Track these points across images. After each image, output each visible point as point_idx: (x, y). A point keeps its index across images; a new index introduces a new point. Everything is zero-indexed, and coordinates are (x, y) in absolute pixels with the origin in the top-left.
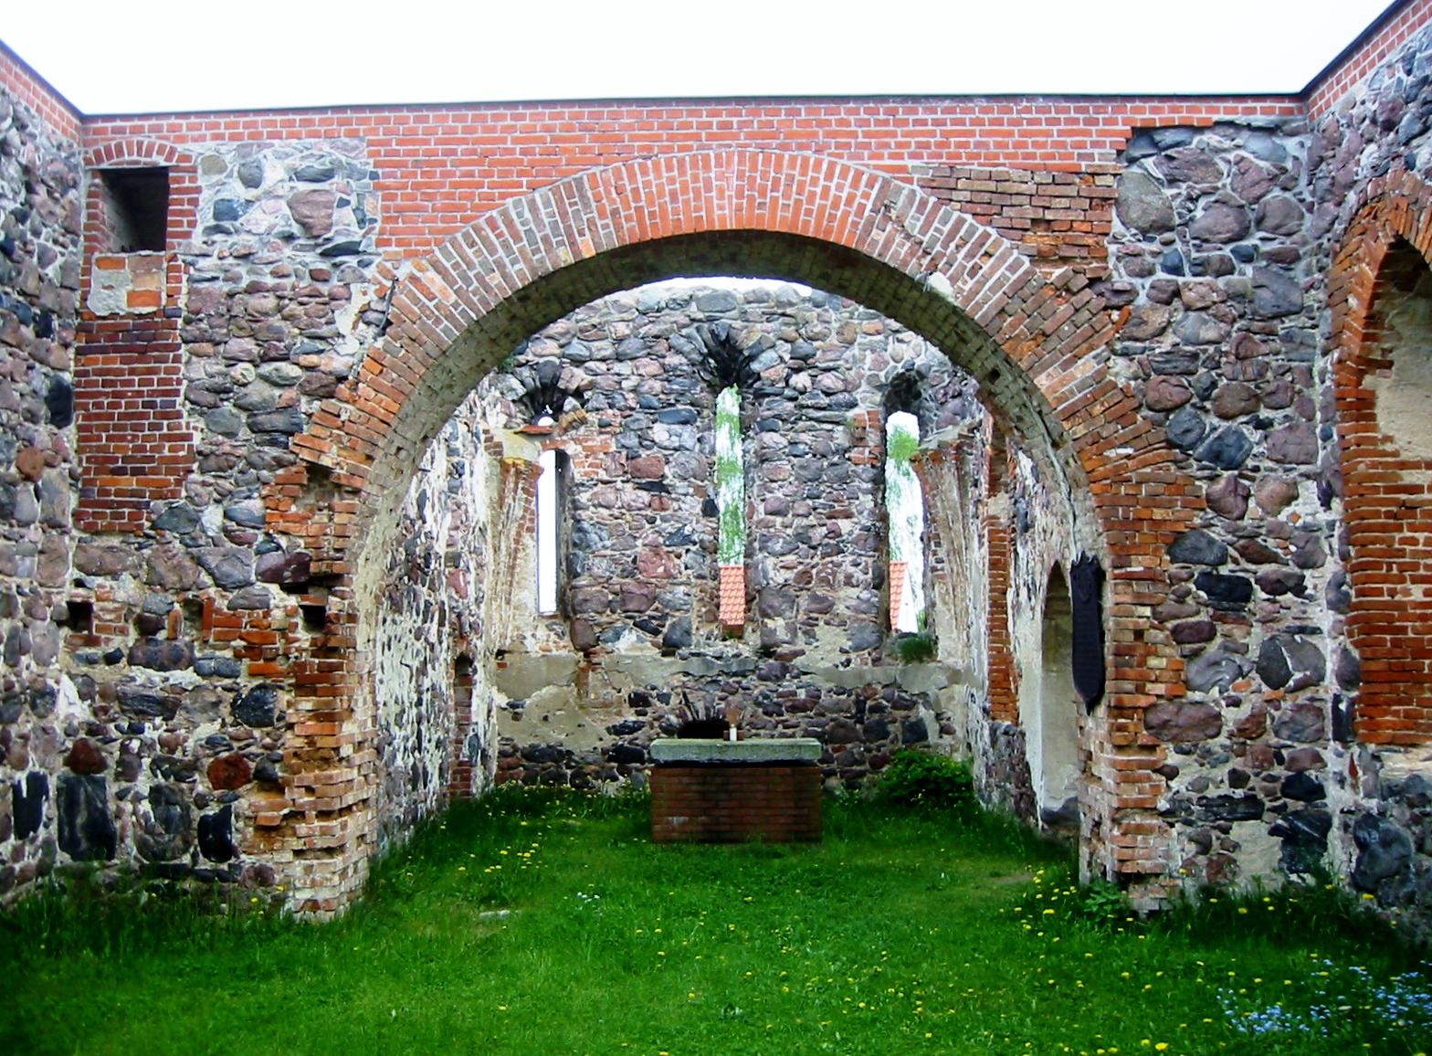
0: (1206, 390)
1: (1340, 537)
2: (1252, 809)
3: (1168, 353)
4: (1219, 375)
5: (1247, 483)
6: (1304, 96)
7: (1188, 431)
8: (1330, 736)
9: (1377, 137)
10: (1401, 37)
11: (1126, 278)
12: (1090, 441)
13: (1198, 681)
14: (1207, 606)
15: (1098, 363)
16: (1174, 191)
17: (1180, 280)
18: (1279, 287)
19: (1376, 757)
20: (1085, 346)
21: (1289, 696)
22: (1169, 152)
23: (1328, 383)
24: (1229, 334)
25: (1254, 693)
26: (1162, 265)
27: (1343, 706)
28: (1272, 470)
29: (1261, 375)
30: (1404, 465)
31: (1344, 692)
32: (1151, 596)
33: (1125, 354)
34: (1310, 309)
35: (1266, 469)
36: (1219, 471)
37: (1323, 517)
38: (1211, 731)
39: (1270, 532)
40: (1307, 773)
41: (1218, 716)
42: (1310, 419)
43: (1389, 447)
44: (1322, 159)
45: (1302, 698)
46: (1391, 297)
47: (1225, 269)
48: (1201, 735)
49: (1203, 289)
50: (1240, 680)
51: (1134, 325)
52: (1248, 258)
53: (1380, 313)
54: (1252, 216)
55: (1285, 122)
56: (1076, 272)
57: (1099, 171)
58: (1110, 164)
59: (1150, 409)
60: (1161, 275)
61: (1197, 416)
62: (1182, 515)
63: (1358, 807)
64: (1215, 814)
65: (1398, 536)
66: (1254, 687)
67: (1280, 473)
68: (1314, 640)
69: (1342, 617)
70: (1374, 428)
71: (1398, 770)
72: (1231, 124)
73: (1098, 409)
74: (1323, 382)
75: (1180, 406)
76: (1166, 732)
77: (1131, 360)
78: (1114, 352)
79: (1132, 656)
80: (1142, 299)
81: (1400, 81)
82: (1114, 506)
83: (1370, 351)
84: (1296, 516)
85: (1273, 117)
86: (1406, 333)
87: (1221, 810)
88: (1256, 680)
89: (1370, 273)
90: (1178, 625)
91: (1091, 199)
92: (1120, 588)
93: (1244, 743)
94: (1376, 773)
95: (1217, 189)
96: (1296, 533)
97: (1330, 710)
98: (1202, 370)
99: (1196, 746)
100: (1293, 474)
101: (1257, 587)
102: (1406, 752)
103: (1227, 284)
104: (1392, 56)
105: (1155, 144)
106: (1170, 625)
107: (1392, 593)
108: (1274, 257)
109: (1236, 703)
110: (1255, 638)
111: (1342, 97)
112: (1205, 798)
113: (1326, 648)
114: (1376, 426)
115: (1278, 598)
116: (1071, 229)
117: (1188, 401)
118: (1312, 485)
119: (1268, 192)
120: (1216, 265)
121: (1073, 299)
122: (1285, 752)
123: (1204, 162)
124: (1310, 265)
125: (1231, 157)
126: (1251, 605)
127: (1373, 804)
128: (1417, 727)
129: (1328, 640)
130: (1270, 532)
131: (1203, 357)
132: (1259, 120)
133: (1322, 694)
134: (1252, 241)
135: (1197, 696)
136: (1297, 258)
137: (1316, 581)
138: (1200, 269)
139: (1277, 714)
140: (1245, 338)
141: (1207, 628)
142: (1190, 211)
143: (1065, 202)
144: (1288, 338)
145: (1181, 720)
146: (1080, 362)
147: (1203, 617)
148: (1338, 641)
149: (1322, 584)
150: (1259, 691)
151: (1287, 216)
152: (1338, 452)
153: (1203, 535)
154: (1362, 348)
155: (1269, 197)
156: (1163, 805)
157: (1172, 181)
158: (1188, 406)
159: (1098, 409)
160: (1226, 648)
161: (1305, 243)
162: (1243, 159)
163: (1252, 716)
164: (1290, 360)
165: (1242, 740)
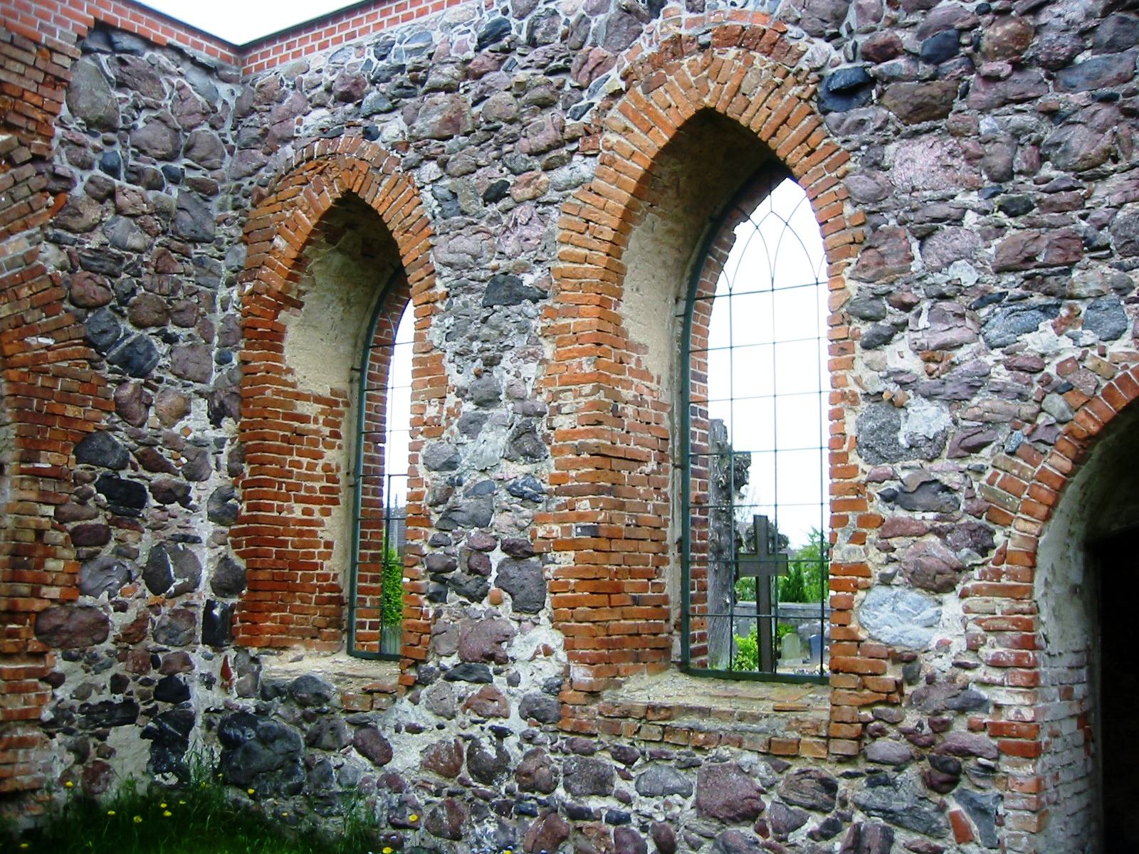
0: (126, 295)
1: (230, 455)
2: (127, 714)
3: (96, 250)
4: (139, 283)
5: (149, 391)
6: (242, 50)
7: (105, 332)
8: (200, 639)
9: (330, 104)
10: (380, 25)
11: (67, 165)
12: (13, 322)
13: (90, 584)
14: (106, 509)
15: (31, 244)
16: (122, 95)
17: (117, 182)
18: (199, 215)
19: (255, 660)
20: (19, 223)
21: (169, 602)
22: (123, 56)
23: (231, 311)
24: (151, 247)
25: (139, 598)
26: (100, 162)
27: (216, 612)
28: (172, 383)
29: (174, 292)
30: (299, 396)
31: (219, 599)
32: (55, 495)
33: (57, 241)
34: (220, 241)
35: (168, 382)
36: (127, 377)
37: (211, 434)
38: (98, 637)
39: (166, 442)
40: (177, 675)
41: (105, 621)
42: (209, 342)
43: (289, 378)
44: (253, 110)
45: (179, 603)
46: (319, 245)
47: (155, 185)
48: (89, 641)
49: (137, 198)
50: (127, 585)
51: (69, 214)
52: (175, 179)
53: (307, 257)
54: (183, 142)
55: (222, 68)
56: (21, 144)
57: (58, 49)
58: (71, 47)
59: (72, 302)
60: (97, 172)
61: (114, 319)
62: (93, 415)
63: (228, 706)
64: (96, 721)
65: (289, 458)
66: (139, 593)
67: (179, 387)
68: (193, 548)
69: (226, 529)
70: (281, 360)
71: (276, 671)
72: (179, 51)
73: (25, 292)
74: (225, 310)
75: (100, 306)
76: (56, 638)
77: (61, 249)
78: (47, 238)
79: (30, 557)
80: (78, 191)
81: (369, 62)
82: (29, 396)
83: (290, 289)
84: (187, 430)
85: (214, 59)
86: (320, 280)
87: (101, 716)
88: (142, 586)
89: (309, 222)
90: (78, 527)
91: (46, 74)
92: (26, 484)
93: (127, 648)
94: (256, 675)
95: (159, 106)
96: (188, 446)
97: (201, 616)
98: (124, 276)
99: (83, 651)
100: (190, 390)
101: (150, 494)
102: (279, 654)
103: (156, 198)
104: (366, 40)
105: (111, 44)
106: (70, 526)
107: (280, 510)
108: (197, 185)
109: (122, 608)
110: (145, 543)
111: (291, 62)
112: (87, 705)
113: (203, 557)
114: (283, 357)
115: (167, 506)
116: (21, 97)
117: (107, 302)
118: (204, 403)
119: (200, 124)
120: (149, 178)
121: (13, 171)
122: (160, 656)
123: (151, 76)
124: (225, 201)
125: (175, 81)
126: (144, 512)
127: (250, 704)
128: (288, 631)
129: (206, 550)
130: (166, 442)
131: (127, 262)
132: (203, 57)
133: (195, 600)
134: (178, 165)
135: (88, 600)
136: (215, 192)
137: (202, 493)
138: (134, 177)
139: (157, 619)
140: (165, 254)
141: (104, 531)
142: (134, 119)
143: (19, 68)
144: (200, 263)
145: (71, 626)
146: (13, 238)
147: (100, 521)
148: (217, 551)
149: (205, 496)
150: (142, 596)
151: (212, 151)
152: (238, 376)
153: (109, 438)
154: (285, 285)
155: (199, 129)
156: (47, 715)
157: (121, 85)
158: (107, 307)
159: (25, 292)
160: (117, 553)
161: (223, 181)
162: (184, 87)
163: (137, 621)
164: (198, 284)
165: (125, 644)
